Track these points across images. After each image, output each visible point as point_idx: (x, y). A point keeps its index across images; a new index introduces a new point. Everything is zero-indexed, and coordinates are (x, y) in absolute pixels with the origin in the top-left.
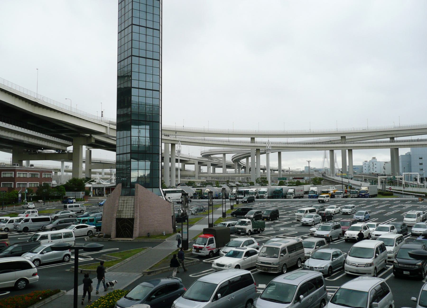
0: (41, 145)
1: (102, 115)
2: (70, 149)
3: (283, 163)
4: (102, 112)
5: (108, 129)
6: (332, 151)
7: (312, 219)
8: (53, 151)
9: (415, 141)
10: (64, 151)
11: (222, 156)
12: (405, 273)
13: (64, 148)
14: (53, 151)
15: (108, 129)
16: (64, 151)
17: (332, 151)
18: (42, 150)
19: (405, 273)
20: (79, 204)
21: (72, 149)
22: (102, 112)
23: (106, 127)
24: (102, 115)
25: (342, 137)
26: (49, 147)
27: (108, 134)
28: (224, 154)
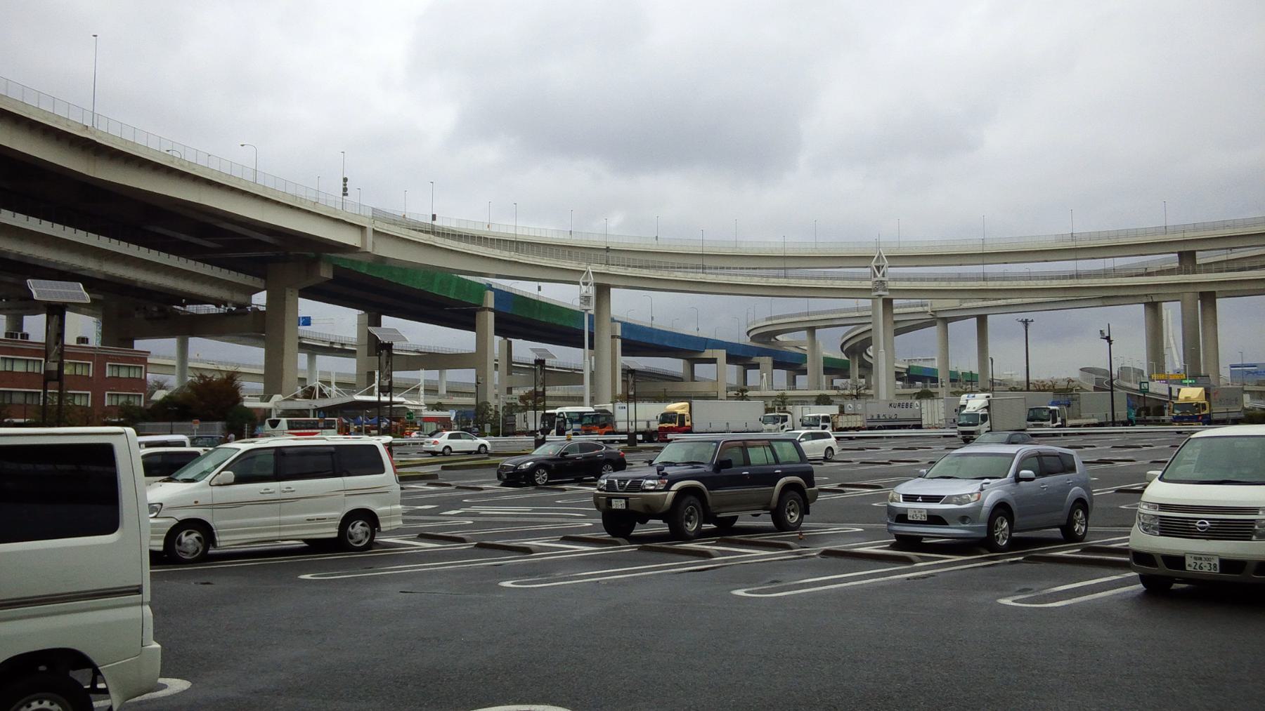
0: (182, 292)
1: (345, 189)
2: (260, 299)
3: (992, 352)
4: (345, 180)
5: (370, 234)
6: (1154, 308)
7: (993, 492)
8: (211, 309)
9: (1088, 275)
10: (242, 307)
11: (803, 336)
12: (1176, 586)
13: (239, 298)
14: (211, 309)
15: (370, 234)
16: (242, 307)
17: (1154, 308)
18: (183, 305)
19: (1176, 586)
20: (380, 441)
21: (264, 302)
22: (345, 180)
23: (362, 228)
24: (345, 189)
25: (1180, 254)
26: (203, 297)
27: (369, 249)
28: (812, 330)
